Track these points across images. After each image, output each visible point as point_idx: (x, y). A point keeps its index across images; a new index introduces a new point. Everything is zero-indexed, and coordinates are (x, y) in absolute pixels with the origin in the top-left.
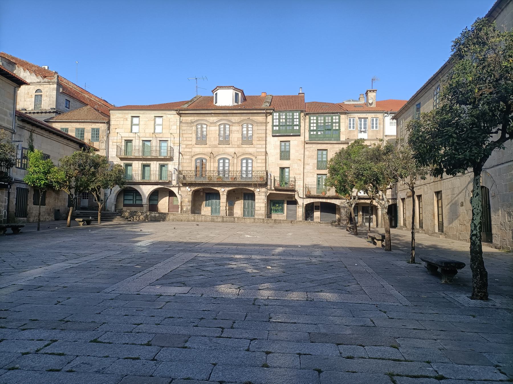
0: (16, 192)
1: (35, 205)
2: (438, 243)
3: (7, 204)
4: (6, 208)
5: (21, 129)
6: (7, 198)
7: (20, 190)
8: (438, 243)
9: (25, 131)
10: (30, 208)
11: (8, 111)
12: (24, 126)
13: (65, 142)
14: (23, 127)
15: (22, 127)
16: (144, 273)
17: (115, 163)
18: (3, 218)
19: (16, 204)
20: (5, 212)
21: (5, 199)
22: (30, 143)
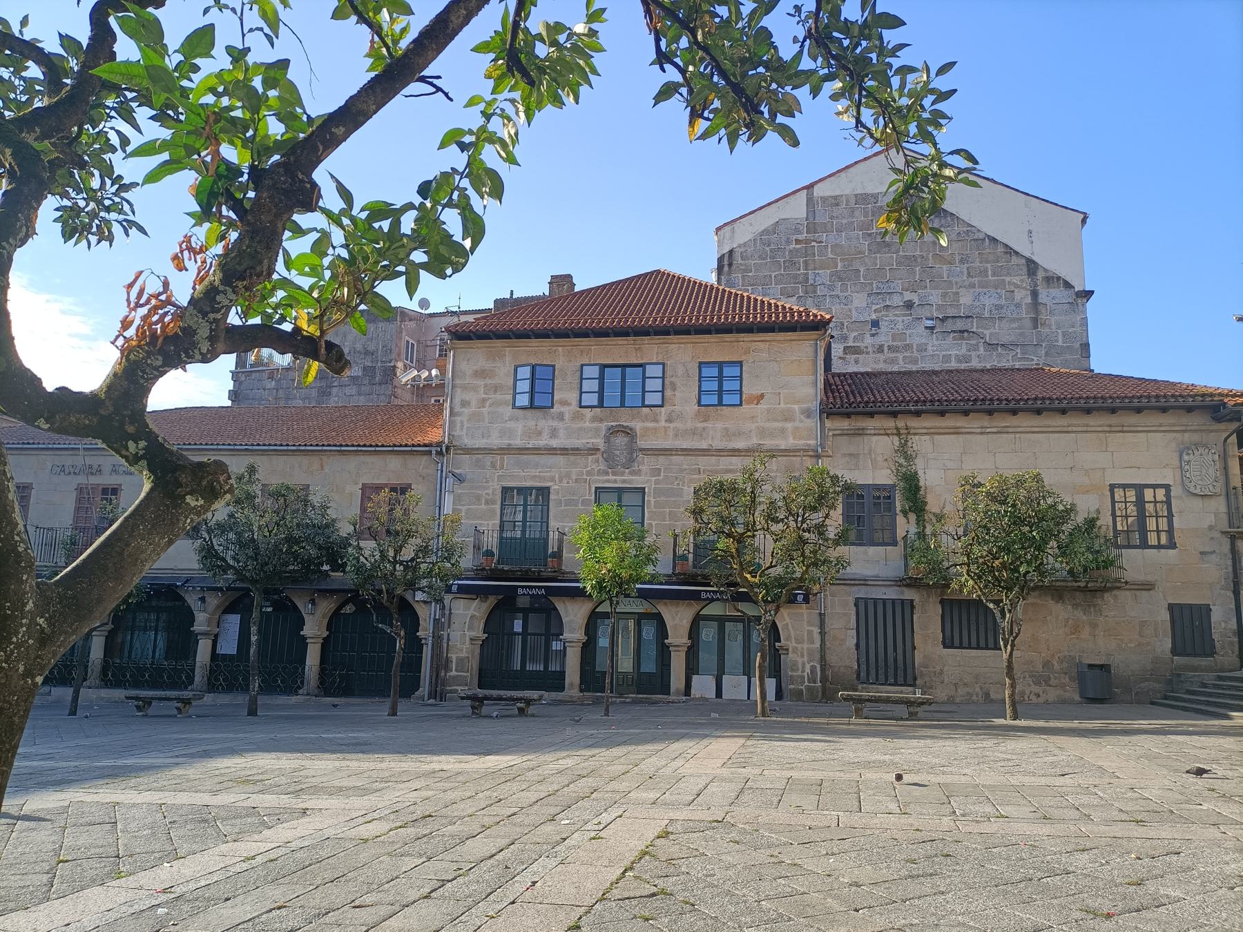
0: (854, 612)
1: (952, 647)
2: (591, 764)
3: (818, 645)
4: (818, 656)
5: (857, 439)
6: (816, 630)
7: (889, 607)
8: (591, 764)
9: (875, 438)
10: (925, 657)
11: (796, 407)
12: (858, 429)
13: (1100, 423)
14: (860, 432)
15: (852, 432)
16: (249, 867)
17: (146, 312)
18: (806, 683)
19: (857, 646)
20: (813, 669)
21: (810, 632)
22: (900, 465)
